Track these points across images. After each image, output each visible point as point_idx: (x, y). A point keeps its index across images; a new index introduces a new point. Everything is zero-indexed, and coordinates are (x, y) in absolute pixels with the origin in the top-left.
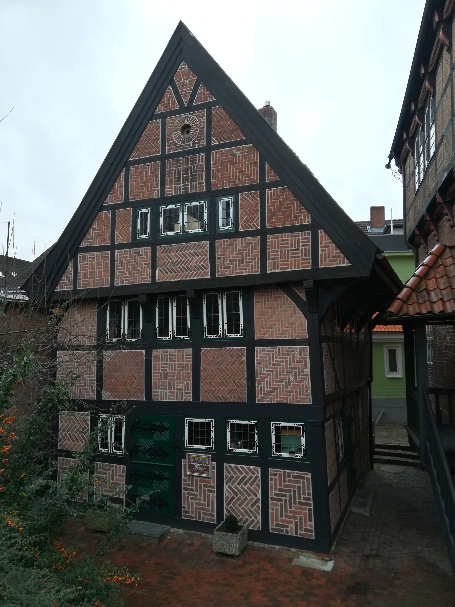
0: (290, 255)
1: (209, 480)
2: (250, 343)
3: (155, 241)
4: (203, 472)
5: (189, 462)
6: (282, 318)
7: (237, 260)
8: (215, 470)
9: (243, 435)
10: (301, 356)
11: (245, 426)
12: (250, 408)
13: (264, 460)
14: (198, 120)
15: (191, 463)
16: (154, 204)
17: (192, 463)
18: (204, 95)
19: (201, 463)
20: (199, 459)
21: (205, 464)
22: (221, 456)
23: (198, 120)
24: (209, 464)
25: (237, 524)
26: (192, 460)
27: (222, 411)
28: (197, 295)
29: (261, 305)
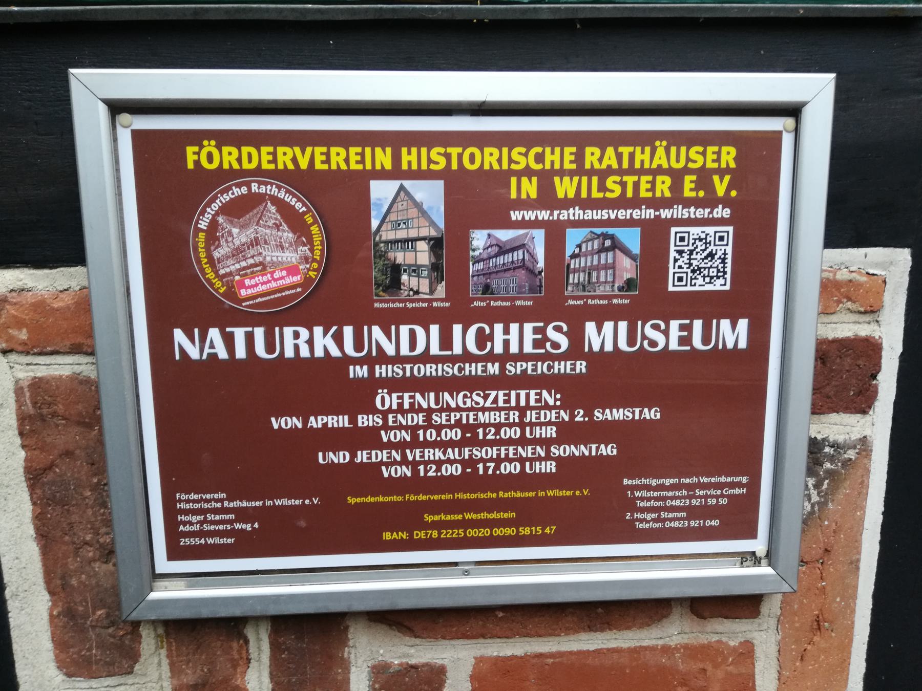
0: (424, 232)
1: (728, 632)
2: (416, 251)
3: (396, 229)
4: (589, 509)
5: (178, 293)
6: (422, 246)
7: (413, 234)
8: (877, 426)
9: (414, 271)
10: (427, 254)
11: (415, 270)
12: (416, 265)
13: (418, 276)
14: (405, 203)
15: (245, 342)
16: (396, 221)
17: (275, 315)
18: (406, 198)
19: (550, 296)
20: (476, 199)
21: (648, 297)
22: (409, 276)
23: (405, 203)
24: (750, 293)
25: (310, 146)
26: (269, 256)
27: (410, 266)
28: (406, 241)
29: (418, 243)
